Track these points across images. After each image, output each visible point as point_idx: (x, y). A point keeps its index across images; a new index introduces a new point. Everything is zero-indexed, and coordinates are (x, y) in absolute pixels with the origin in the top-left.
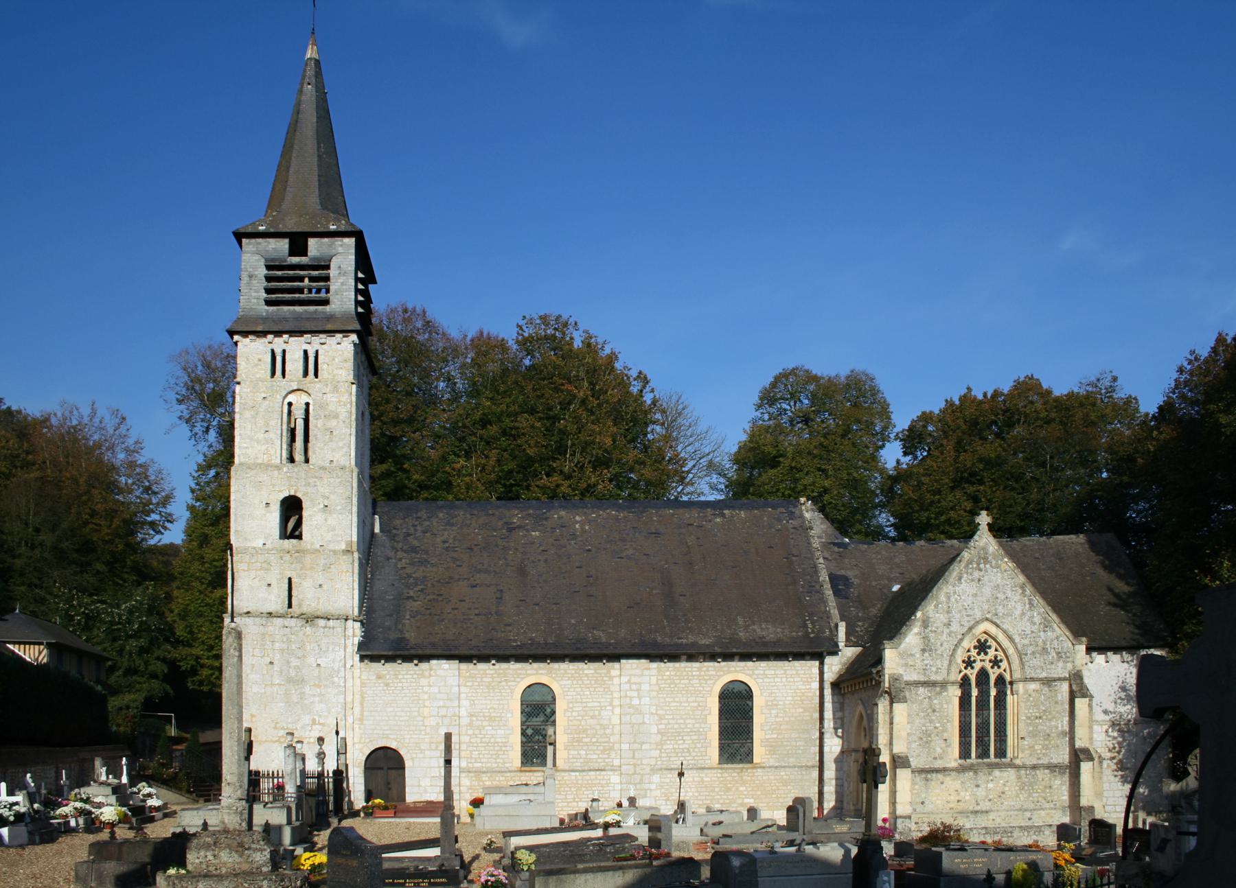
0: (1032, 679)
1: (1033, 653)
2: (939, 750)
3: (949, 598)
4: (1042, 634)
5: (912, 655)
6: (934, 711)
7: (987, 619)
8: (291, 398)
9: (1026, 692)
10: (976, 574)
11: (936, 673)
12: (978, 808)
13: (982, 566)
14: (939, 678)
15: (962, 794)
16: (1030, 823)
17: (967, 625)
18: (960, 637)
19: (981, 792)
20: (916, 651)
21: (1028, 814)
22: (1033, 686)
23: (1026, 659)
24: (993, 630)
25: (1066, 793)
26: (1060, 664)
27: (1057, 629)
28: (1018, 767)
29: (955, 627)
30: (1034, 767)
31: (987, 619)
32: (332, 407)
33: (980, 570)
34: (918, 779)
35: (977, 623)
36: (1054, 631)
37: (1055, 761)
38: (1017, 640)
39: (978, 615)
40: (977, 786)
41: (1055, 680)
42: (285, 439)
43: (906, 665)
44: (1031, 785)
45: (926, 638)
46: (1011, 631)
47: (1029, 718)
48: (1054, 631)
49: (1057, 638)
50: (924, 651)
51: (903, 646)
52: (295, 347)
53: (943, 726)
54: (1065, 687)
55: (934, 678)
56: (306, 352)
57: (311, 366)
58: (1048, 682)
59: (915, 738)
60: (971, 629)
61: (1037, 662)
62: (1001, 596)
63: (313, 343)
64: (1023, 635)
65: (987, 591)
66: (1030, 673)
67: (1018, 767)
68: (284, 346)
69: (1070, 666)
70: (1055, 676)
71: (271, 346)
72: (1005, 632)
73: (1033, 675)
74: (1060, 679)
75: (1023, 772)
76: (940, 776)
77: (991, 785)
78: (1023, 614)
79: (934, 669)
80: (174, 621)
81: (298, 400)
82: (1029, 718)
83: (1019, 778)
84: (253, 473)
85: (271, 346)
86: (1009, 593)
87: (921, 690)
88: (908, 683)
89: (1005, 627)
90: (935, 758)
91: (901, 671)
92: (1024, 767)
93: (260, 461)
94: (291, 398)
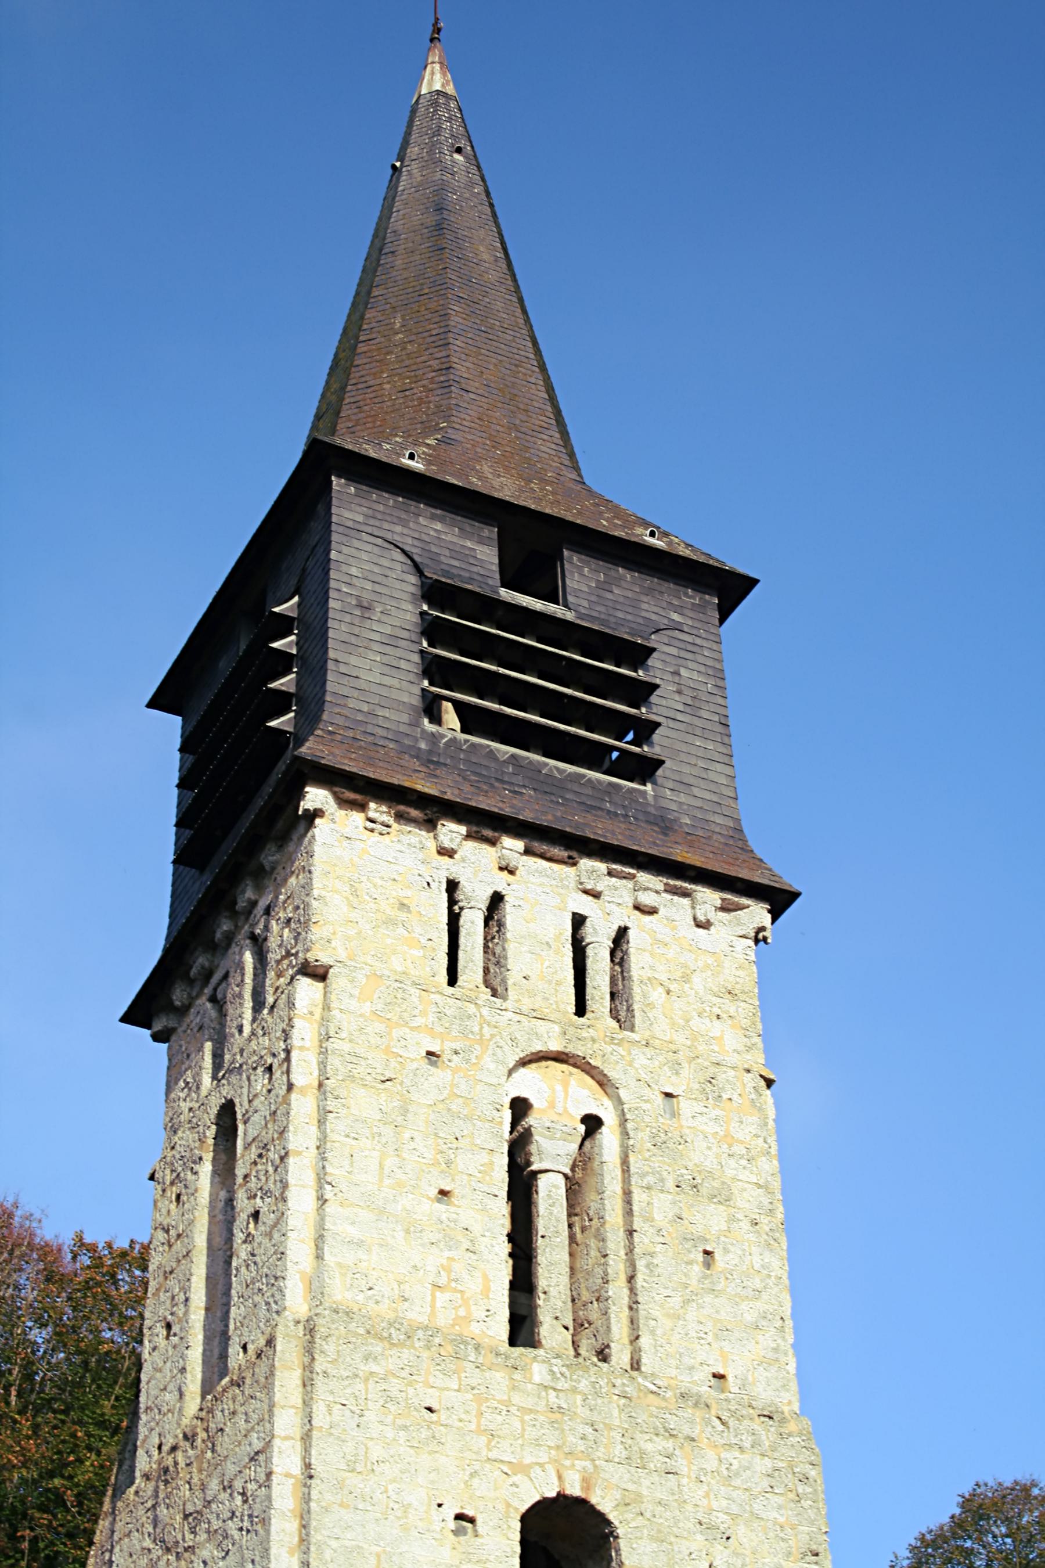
8: (530, 1083)
42: (613, 1185)
52: (544, 895)
56: (578, 921)
57: (597, 973)
63: (614, 898)
68: (500, 882)
71: (447, 868)
80: (147, 1477)
81: (560, 1101)
84: (394, 1360)
85: (447, 868)
93: (417, 1314)
94: (530, 1083)
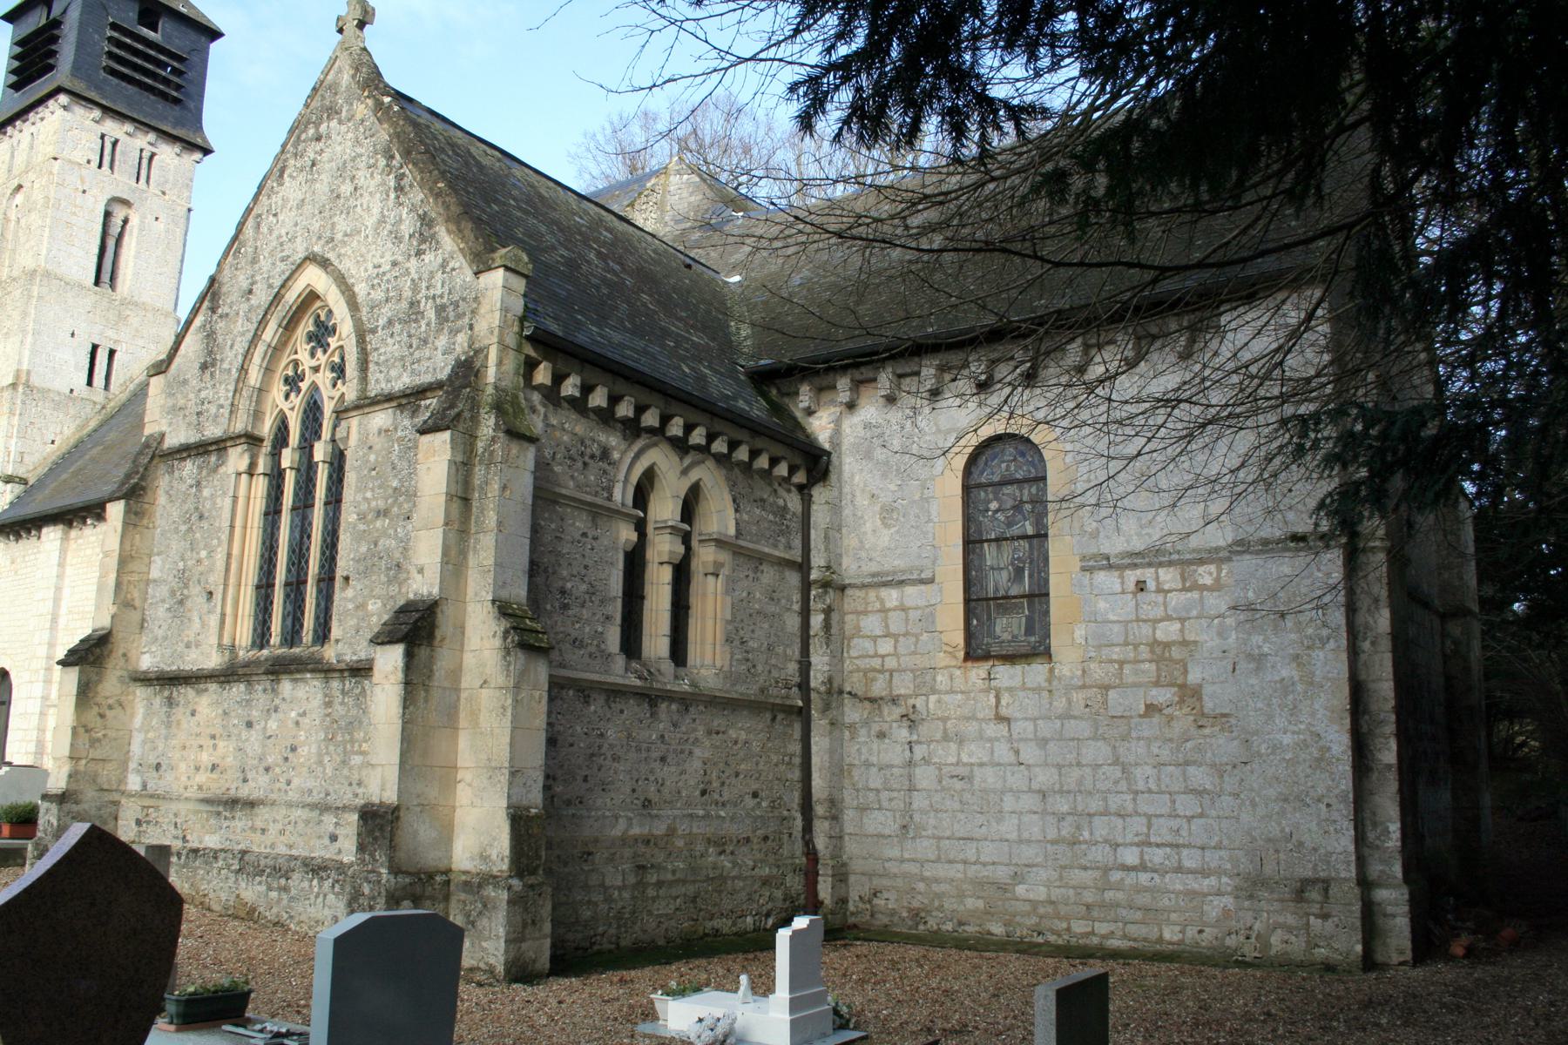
38: (361, 289)
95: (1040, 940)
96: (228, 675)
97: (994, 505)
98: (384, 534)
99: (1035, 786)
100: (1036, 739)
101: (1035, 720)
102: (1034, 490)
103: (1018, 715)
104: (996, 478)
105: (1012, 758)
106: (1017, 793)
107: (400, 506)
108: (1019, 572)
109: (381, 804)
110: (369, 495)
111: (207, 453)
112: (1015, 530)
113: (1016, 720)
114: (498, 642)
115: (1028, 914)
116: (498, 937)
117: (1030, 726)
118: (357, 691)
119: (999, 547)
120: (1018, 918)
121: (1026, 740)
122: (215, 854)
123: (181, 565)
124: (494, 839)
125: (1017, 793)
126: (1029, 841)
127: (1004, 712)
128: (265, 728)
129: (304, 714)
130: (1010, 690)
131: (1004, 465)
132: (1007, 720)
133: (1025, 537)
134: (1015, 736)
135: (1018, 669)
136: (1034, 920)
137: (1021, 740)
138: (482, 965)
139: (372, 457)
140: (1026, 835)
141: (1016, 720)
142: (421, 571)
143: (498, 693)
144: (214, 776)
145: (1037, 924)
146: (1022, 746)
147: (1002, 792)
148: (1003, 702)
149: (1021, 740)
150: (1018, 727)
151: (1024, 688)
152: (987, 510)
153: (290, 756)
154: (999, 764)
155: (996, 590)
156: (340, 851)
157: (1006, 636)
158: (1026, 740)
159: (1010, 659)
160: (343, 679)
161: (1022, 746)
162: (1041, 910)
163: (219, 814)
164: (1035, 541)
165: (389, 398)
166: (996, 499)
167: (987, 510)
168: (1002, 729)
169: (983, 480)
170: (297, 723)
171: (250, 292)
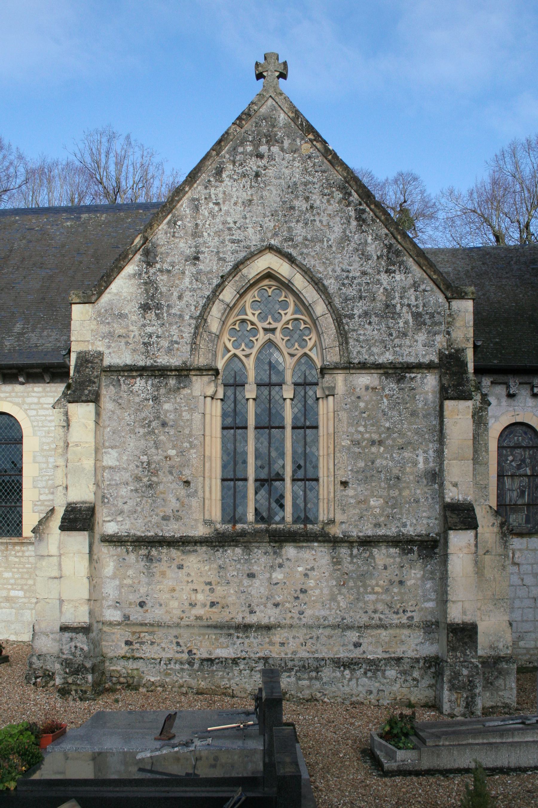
0: (364, 366)
1: (366, 314)
2: (174, 504)
3: (196, 208)
4: (384, 277)
5: (122, 316)
6: (164, 424)
7: (271, 248)
9: (351, 390)
10: (253, 164)
11: (169, 350)
12: (252, 619)
13: (263, 149)
14: (175, 361)
15: (219, 590)
16: (356, 653)
17: (231, 260)
18: (215, 282)
19: (258, 588)
20: (132, 309)
21: (353, 636)
22: (364, 380)
23: (350, 325)
24: (284, 269)
25: (306, 295)
26: (422, 337)
27: (415, 268)
28: (334, 542)
29: (209, 263)
30: (367, 542)
31: (271, 248)
32: (320, 788)
33: (260, 156)
34: (132, 558)
35: (251, 256)
36: (407, 271)
37: (410, 530)
38: (331, 284)
39: (254, 239)
40: (251, 576)
41: (409, 367)
43: (110, 335)
44: (363, 577)
45: (149, 285)
46: (319, 269)
47: (357, 443)
48: (407, 271)
49: (415, 286)
50: (145, 308)
51: (105, 298)
53: (181, 453)
54: (430, 382)
55: (163, 360)
58: (399, 371)
59: (126, 476)
60: (237, 267)
61: (371, 331)
62: (300, 204)
64: (345, 280)
65: (273, 196)
66: (358, 353)
67: (334, 542)
69: (440, 340)
70: (412, 360)
72: (306, 272)
73: (365, 357)
74: (419, 367)
75: (344, 551)
76: (174, 553)
77: (278, 576)
78: (345, 239)
79: (165, 344)
82: (357, 443)
83: (337, 562)
86: (317, 200)
87: (139, 384)
88: (112, 370)
89: (309, 262)
90: (165, 518)
91: (100, 346)
92: (346, 541)
95: (531, 665)
96: (218, 541)
97: (510, 458)
98: (381, 456)
99: (531, 595)
100: (532, 573)
101: (532, 564)
102: (531, 452)
103: (523, 562)
104: (512, 444)
105: (520, 583)
106: (521, 599)
107: (394, 440)
108: (523, 493)
109: (463, 623)
110: (361, 429)
111: (166, 377)
112: (521, 471)
113: (523, 564)
114: (496, 529)
115: (525, 654)
116: (511, 689)
117: (530, 567)
118: (367, 555)
119: (512, 479)
120: (520, 657)
121: (527, 574)
122: (235, 661)
123: (145, 458)
124: (501, 637)
125: (521, 599)
126: (527, 621)
127: (516, 560)
128: (270, 578)
129: (313, 569)
130: (520, 550)
131: (516, 438)
132: (518, 564)
133: (526, 475)
134: (522, 572)
135: (525, 540)
136: (528, 657)
137: (524, 574)
138: (499, 704)
139: (362, 405)
140: (525, 618)
141: (523, 564)
142: (455, 485)
143: (498, 558)
144: (214, 609)
145: (530, 659)
146: (525, 577)
147: (514, 599)
148: (516, 556)
149: (524, 574)
150: (523, 568)
151: (527, 549)
152: (507, 460)
153: (301, 596)
154: (513, 586)
155: (510, 500)
156: (364, 652)
157: (515, 524)
158: (527, 574)
159: (521, 535)
160: (351, 547)
161: (525, 577)
162: (532, 652)
163: (230, 635)
164: (531, 478)
165: (377, 366)
166: (512, 455)
167: (507, 460)
168: (515, 569)
169: (505, 445)
170: (306, 575)
171: (197, 258)
